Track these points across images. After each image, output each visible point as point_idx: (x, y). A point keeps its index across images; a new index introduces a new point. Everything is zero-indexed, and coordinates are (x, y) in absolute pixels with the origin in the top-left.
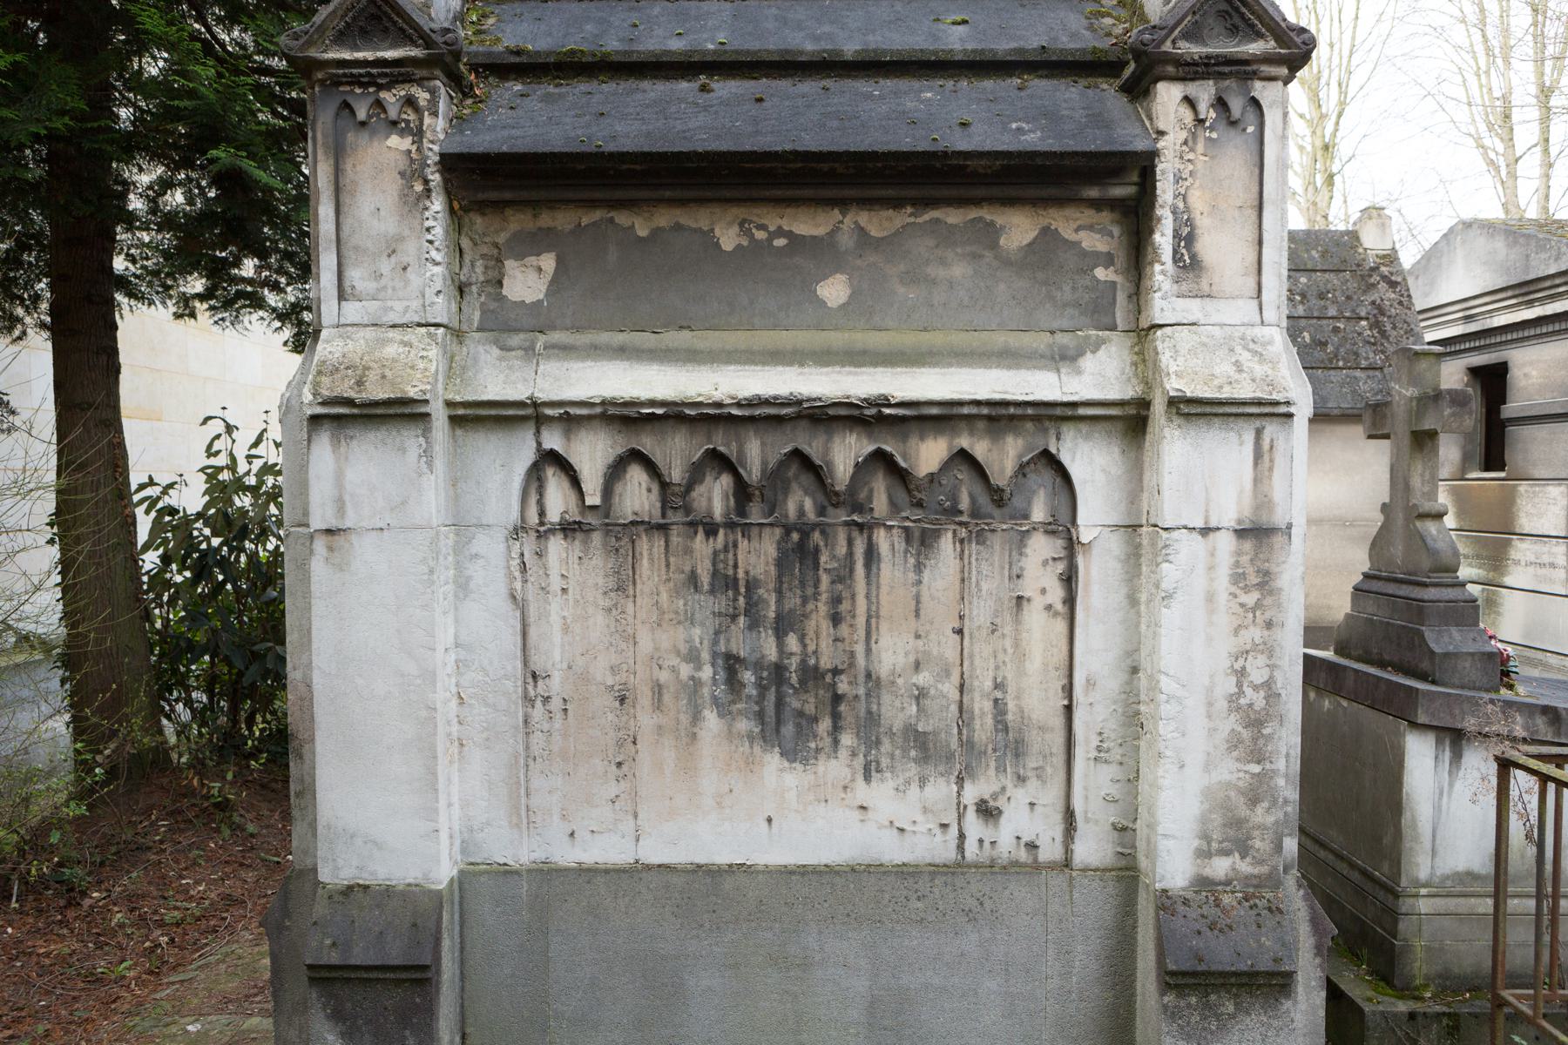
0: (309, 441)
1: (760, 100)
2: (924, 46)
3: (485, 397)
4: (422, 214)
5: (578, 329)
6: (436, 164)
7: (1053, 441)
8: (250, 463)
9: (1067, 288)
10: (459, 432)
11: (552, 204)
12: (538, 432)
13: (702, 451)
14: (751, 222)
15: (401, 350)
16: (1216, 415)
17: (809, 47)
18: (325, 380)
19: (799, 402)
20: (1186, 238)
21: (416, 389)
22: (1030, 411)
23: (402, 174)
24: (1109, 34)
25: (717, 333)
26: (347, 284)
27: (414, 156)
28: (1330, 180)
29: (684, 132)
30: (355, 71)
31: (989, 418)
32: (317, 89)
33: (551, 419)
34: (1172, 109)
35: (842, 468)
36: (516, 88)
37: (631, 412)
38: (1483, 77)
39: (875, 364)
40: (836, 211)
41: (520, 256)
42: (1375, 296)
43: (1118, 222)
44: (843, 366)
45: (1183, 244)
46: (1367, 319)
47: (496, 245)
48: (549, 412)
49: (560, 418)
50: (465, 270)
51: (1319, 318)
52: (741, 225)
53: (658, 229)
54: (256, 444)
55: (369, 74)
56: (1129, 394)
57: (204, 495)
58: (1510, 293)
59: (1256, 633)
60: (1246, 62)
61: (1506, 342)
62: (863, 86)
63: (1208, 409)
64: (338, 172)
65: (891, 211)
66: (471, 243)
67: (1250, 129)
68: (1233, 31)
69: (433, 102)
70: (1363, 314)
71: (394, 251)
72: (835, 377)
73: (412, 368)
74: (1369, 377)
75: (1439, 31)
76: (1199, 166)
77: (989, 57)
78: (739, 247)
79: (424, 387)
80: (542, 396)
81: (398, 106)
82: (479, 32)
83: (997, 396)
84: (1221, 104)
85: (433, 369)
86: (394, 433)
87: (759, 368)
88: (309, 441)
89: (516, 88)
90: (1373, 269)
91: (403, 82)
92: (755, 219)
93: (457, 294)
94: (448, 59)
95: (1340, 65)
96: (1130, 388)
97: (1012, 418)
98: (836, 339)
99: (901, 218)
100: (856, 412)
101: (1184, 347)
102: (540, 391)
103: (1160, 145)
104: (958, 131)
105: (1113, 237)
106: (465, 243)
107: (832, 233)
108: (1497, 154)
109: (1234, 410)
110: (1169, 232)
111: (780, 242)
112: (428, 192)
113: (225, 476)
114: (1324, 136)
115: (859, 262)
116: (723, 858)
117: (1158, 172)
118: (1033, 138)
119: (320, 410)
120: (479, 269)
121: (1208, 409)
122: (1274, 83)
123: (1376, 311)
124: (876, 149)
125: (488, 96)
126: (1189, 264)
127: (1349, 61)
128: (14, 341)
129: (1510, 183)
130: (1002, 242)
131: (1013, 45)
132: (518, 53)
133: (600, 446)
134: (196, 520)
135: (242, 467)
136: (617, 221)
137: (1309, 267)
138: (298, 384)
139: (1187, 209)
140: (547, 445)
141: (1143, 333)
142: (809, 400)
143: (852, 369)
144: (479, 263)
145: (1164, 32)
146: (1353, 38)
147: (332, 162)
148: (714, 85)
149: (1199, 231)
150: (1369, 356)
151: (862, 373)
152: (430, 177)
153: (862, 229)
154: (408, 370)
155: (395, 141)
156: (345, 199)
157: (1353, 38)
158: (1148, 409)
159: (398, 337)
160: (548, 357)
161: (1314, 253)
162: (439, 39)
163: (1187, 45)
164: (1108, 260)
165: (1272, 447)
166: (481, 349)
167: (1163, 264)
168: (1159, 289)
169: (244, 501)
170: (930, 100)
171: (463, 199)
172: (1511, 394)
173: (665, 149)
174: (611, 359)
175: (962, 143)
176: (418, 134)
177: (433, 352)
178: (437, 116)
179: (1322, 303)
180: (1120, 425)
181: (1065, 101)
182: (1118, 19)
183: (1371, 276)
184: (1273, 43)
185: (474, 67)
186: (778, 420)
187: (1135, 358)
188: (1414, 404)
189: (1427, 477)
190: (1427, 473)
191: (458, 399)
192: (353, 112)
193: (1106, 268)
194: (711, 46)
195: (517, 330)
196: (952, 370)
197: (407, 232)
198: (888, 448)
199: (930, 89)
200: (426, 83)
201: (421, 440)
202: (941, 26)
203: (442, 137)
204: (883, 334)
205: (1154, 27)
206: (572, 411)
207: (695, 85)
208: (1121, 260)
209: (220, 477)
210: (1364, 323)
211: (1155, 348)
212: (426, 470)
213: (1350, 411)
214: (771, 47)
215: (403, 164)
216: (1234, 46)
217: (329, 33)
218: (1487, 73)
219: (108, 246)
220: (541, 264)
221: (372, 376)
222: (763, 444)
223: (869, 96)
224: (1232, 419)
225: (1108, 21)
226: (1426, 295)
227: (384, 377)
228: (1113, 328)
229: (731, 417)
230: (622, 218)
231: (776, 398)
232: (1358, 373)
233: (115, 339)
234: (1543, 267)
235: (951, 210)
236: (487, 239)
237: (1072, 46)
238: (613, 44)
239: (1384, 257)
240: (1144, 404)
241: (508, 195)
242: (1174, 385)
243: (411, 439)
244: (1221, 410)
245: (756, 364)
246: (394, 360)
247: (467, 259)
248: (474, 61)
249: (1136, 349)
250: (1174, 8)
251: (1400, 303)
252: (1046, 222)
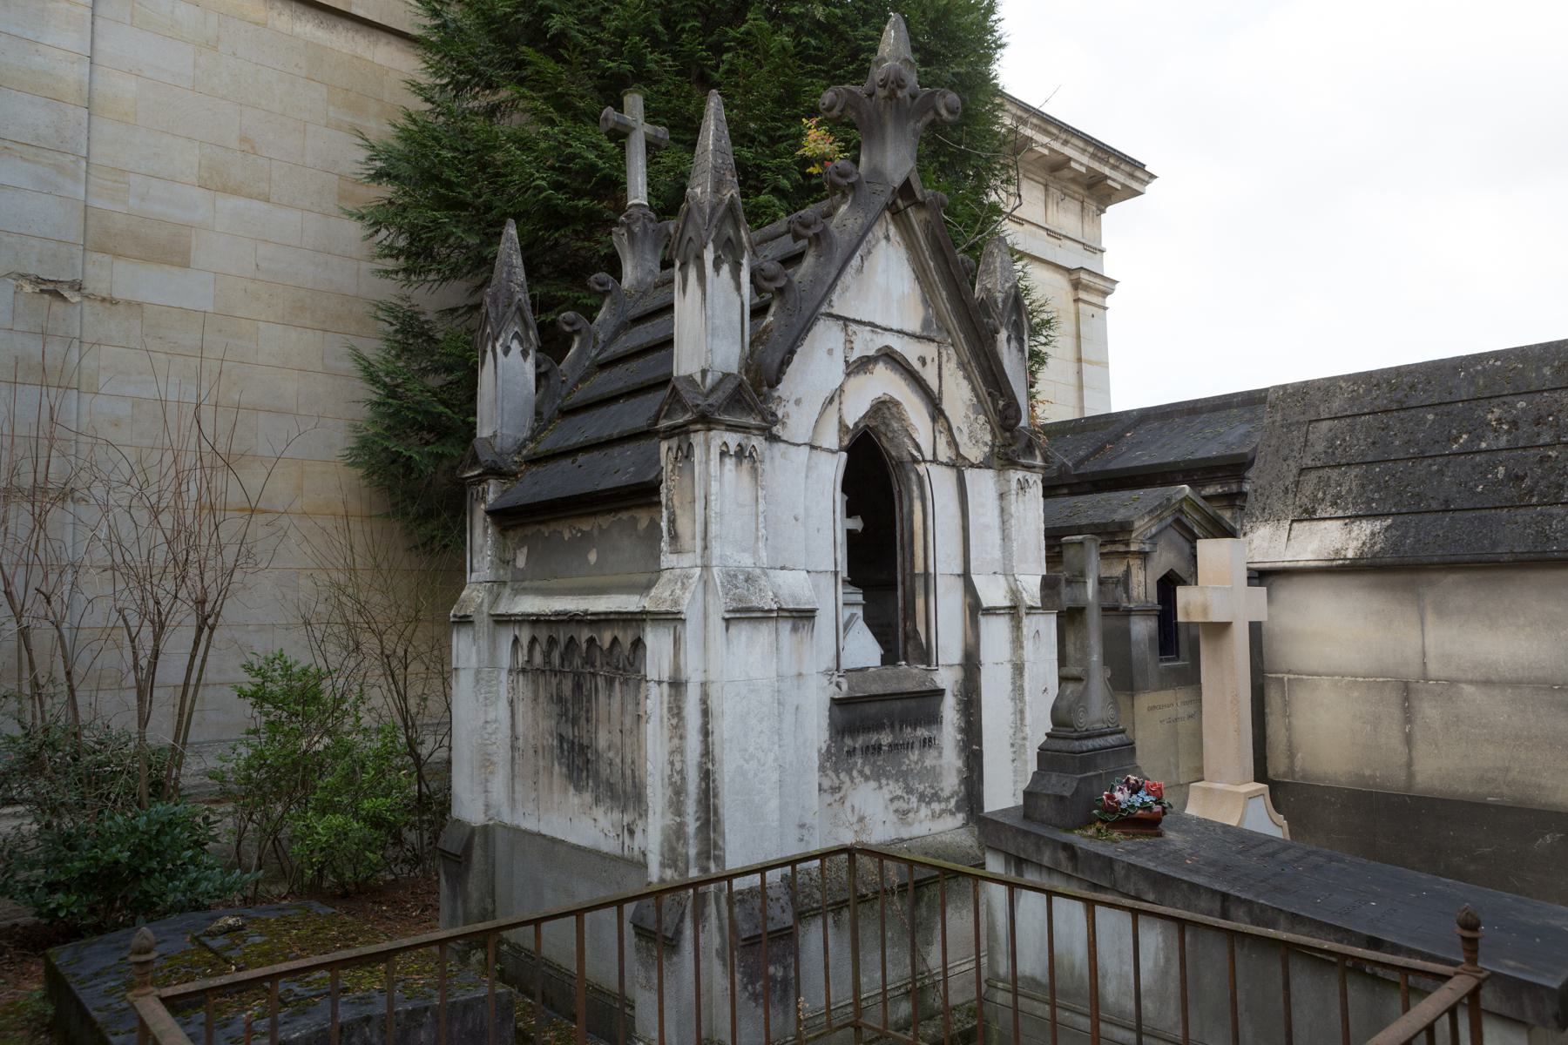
10: (497, 627)
51: (1524, 448)
59: (676, 741)
116: (560, 836)
189: (1078, 645)
190: (1078, 643)
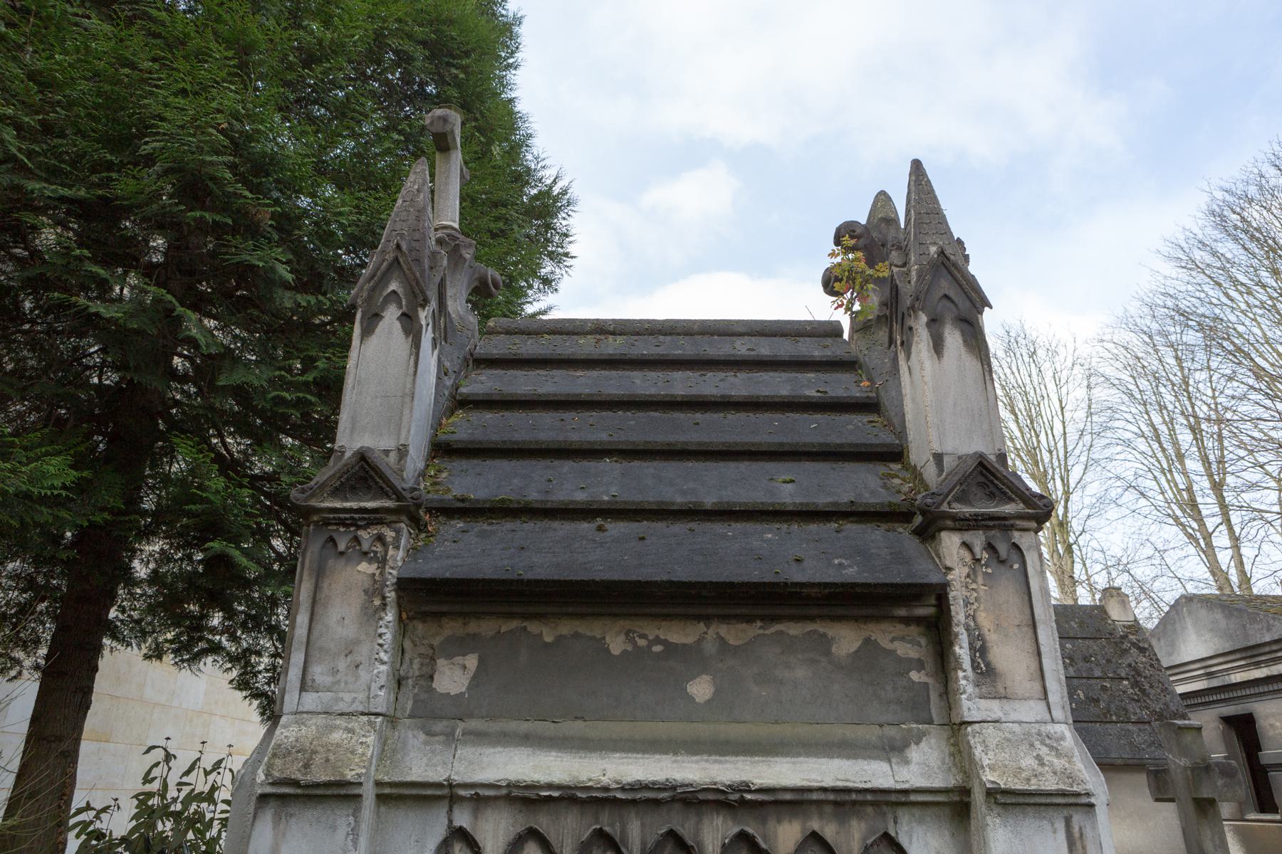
0: (255, 817)
1: (642, 539)
2: (764, 500)
3: (409, 779)
4: (377, 622)
5: (491, 717)
6: (393, 584)
7: (891, 824)
8: (179, 791)
9: (889, 688)
10: (383, 809)
11: (478, 616)
12: (451, 810)
13: (590, 831)
14: (634, 632)
15: (344, 736)
16: (1028, 804)
17: (679, 499)
18: (278, 762)
19: (674, 788)
20: (980, 650)
21: (354, 773)
22: (869, 797)
23: (366, 592)
24: (899, 492)
25: (606, 723)
26: (309, 677)
27: (377, 578)
28: (1069, 549)
29: (585, 563)
30: (342, 516)
31: (836, 803)
32: (312, 527)
33: (462, 799)
34: (955, 551)
35: (710, 848)
36: (458, 525)
37: (531, 794)
38: (1168, 475)
39: (736, 753)
40: (702, 624)
41: (450, 656)
42: (1129, 660)
43: (924, 635)
44: (710, 755)
45: (978, 654)
46: (1127, 679)
47: (432, 647)
48: (462, 793)
49: (471, 799)
50: (405, 666)
51: (1088, 678)
52: (627, 634)
53: (561, 636)
54: (187, 773)
55: (352, 518)
56: (951, 782)
57: (132, 819)
58: (1238, 656)
60: (1005, 519)
61: (1247, 696)
62: (719, 528)
63: (1021, 800)
64: (317, 588)
65: (744, 625)
66: (411, 644)
67: (1016, 566)
68: (991, 496)
69: (397, 539)
70: (1123, 675)
71: (351, 652)
72: (703, 764)
73: (352, 752)
74: (1140, 730)
75: (1128, 444)
76: (982, 593)
77: (812, 508)
78: (625, 652)
79: (359, 771)
80: (457, 778)
81: (370, 541)
82: (435, 484)
83: (840, 784)
84: (990, 547)
85: (369, 754)
86: (329, 812)
87: (640, 756)
88: (255, 817)
89: (458, 525)
90: (1125, 637)
91: (377, 524)
92: (638, 630)
93: (396, 686)
94: (412, 509)
95: (1060, 465)
96: (951, 777)
97: (854, 803)
98: (703, 730)
99: (755, 630)
100: (722, 797)
101: (992, 742)
102: (457, 773)
103: (950, 577)
104: (794, 565)
105: (921, 646)
106: (408, 644)
107: (700, 640)
108: (1193, 529)
109: (1043, 800)
110: (966, 645)
111: (657, 649)
112: (384, 606)
113: (155, 801)
114: (1058, 516)
115: (720, 665)
117: (951, 599)
118: (851, 573)
119: (269, 790)
120: (416, 666)
121: (1021, 800)
122: (1028, 533)
123: (1133, 673)
124: (732, 580)
125: (437, 531)
126: (986, 673)
127: (1066, 463)
128: (9, 680)
129: (1210, 552)
130: (834, 649)
131: (830, 500)
132: (463, 501)
133: (503, 825)
134: (119, 845)
135: (172, 793)
136: (529, 629)
137: (1071, 635)
138: (254, 762)
139: (977, 627)
140: (457, 823)
141: (956, 729)
142: (683, 785)
143: (718, 758)
144: (416, 661)
145: (942, 497)
146: (1065, 447)
147: (313, 581)
148: (608, 526)
149: (989, 645)
150: (1136, 711)
151: (726, 762)
152: (388, 595)
153: (722, 638)
154: (349, 755)
155: (364, 567)
156: (319, 609)
157: (1065, 447)
158: (969, 796)
159: (344, 725)
160: (465, 743)
161: (1073, 623)
162: (408, 495)
163: (960, 506)
164: (920, 666)
165: (1081, 835)
166: (410, 734)
167: (965, 671)
168: (965, 692)
169: (165, 827)
170: (770, 540)
171: (410, 611)
172: (1263, 742)
173: (571, 578)
174: (518, 745)
175: (797, 576)
176: (383, 562)
177: (371, 739)
178: (399, 549)
179: (1088, 665)
180: (947, 810)
181: (872, 541)
182: (903, 479)
183: (1123, 643)
184: (1022, 505)
185: (429, 510)
186: (656, 803)
187: (952, 749)
188: (1189, 773)
190: (1216, 838)
191: (386, 779)
192: (335, 545)
193: (919, 672)
194: (606, 498)
195: (441, 718)
196: (801, 759)
197: (364, 637)
198: (750, 830)
199: (770, 531)
200: (394, 525)
201: (351, 818)
202: (775, 484)
203: (400, 564)
204: (741, 726)
205: (933, 494)
206: (483, 792)
207: (593, 525)
208: (930, 665)
209: (150, 803)
210: (1125, 682)
211: (968, 743)
212: (351, 848)
213: (1131, 762)
214: (651, 499)
215: (367, 583)
216: (994, 507)
217: (328, 489)
218: (1170, 471)
219: (111, 598)
220: (466, 663)
221: (318, 759)
222: (643, 825)
223: (724, 537)
224: (1042, 808)
225: (897, 481)
226: (1170, 654)
227: (327, 760)
228: (930, 722)
229: (615, 800)
230: (533, 627)
231: (654, 783)
232: (1130, 727)
233: (92, 680)
234: (1258, 636)
235: (791, 624)
236: (425, 642)
237: (873, 500)
238: (533, 495)
239: (1130, 627)
240: (965, 791)
241: (445, 608)
242: (989, 777)
243: (342, 819)
244: (1032, 800)
245: (638, 753)
246: (338, 745)
247: (407, 657)
248: (430, 505)
249: (952, 741)
250: (946, 478)
251: (1152, 665)
252: (867, 634)
